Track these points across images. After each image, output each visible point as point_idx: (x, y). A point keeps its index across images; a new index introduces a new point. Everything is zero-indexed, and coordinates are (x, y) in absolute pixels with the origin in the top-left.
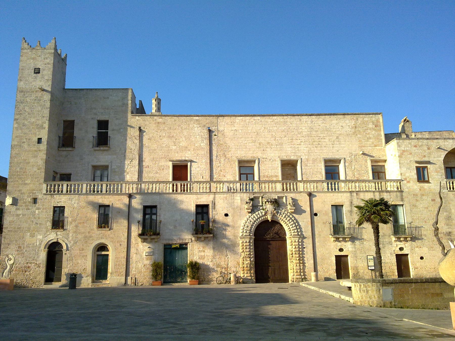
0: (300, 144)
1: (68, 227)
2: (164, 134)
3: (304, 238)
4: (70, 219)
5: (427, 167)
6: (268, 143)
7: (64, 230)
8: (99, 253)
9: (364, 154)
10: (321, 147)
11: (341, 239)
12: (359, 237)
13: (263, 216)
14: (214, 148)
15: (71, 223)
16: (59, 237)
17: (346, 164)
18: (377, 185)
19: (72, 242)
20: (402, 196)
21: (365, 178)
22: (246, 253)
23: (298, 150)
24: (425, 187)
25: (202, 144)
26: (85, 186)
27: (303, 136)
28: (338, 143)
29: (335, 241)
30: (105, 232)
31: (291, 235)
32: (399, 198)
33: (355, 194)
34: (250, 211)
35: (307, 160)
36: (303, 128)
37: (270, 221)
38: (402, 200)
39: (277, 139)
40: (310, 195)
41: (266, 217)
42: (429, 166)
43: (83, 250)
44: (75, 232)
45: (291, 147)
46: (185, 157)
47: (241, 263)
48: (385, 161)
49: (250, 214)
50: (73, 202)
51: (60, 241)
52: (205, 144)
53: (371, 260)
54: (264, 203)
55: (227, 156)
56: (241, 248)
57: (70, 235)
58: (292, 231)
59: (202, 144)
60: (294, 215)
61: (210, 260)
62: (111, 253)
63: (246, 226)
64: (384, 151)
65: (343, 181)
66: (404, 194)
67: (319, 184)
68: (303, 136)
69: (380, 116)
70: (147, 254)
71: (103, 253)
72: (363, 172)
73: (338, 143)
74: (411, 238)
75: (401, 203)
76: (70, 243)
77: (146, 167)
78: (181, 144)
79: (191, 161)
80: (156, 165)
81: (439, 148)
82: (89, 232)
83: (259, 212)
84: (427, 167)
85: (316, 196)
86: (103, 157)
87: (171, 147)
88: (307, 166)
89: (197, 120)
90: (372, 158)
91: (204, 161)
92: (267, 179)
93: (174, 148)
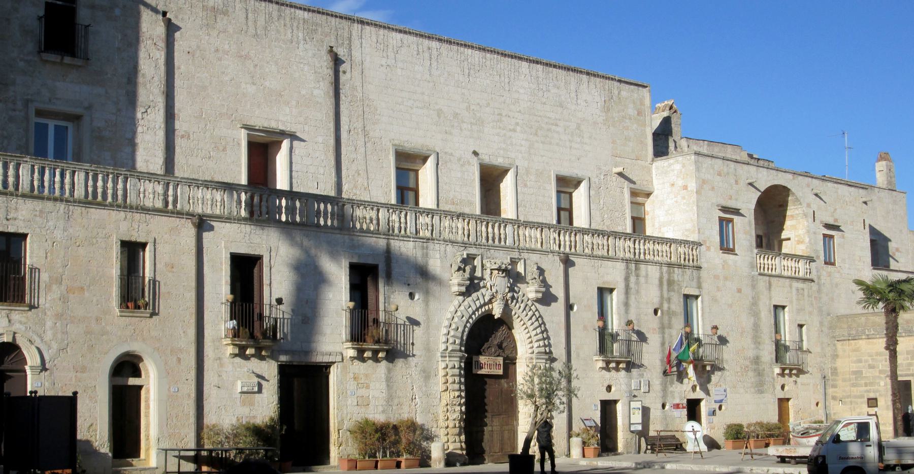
0: (514, 130)
1: (42, 301)
2: (226, 47)
3: (553, 360)
4: (44, 277)
5: (731, 220)
6: (456, 115)
7: (32, 307)
8: (120, 381)
9: (620, 174)
10: (550, 143)
11: (367, 354)
12: (637, 362)
13: (485, 304)
14: (343, 108)
15: (49, 288)
16: (16, 327)
17: (592, 193)
18: (490, 229)
19: (55, 346)
20: (699, 278)
21: (619, 229)
22: (452, 394)
23: (512, 144)
24: (730, 262)
25: (316, 92)
26: (24, 172)
27: (520, 112)
28: (579, 140)
29: (236, 355)
30: (140, 323)
31: (533, 353)
32: (694, 284)
33: (633, 266)
34: (463, 289)
35: (528, 171)
36: (522, 91)
37: (496, 317)
38: (699, 287)
39: (472, 107)
40: (567, 262)
41: (490, 306)
42: (736, 218)
43: (84, 369)
44: (59, 316)
45: (498, 135)
46: (278, 121)
47: (441, 417)
48: (648, 195)
49: (461, 298)
50: (51, 223)
51: (21, 342)
52: (322, 91)
53: (637, 411)
54: (488, 271)
55: (371, 134)
56: (442, 380)
57: (49, 324)
58: (536, 345)
59: (316, 92)
60: (537, 304)
61: (381, 409)
62: (152, 384)
63: (454, 326)
64: (649, 172)
65: (429, 212)
66: (703, 273)
67: (620, 243)
68: (520, 112)
69: (645, 93)
70: (245, 389)
71: (132, 381)
72: (617, 214)
73: (579, 140)
74: (387, 351)
75: (696, 293)
76: (50, 348)
77: (182, 137)
78: (267, 84)
79: (293, 137)
80: (208, 134)
81: (751, 184)
82: (98, 319)
83: (479, 293)
84: (731, 220)
85: (211, 228)
86: (65, 88)
87: (243, 86)
88: (526, 185)
89: (305, 21)
90: (632, 186)
91: (320, 139)
92: (452, 208)
93: (251, 89)
